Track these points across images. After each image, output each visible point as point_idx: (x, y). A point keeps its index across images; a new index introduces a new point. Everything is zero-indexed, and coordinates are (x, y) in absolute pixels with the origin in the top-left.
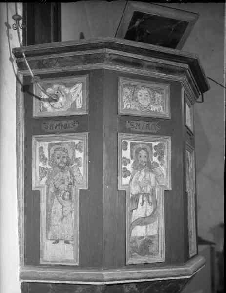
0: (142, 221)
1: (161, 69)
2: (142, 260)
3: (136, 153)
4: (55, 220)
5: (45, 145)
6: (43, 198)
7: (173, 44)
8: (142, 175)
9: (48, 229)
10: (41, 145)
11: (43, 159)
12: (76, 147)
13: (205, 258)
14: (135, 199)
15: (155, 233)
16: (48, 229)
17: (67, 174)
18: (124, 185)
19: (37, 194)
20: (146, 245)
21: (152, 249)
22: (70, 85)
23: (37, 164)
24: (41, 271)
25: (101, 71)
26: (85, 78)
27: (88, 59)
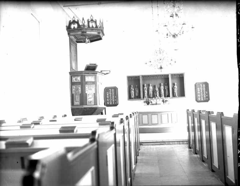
0: (90, 98)
1: (92, 73)
2: (90, 104)
3: (89, 88)
4: (76, 98)
5: (74, 86)
6: (74, 94)
7: (94, 70)
8: (144, 100)
9: (75, 100)
10: (74, 87)
11: (74, 89)
12: (79, 87)
13: (208, 164)
14: (89, 95)
15: (92, 100)
16: (75, 100)
17: (78, 91)
18: (157, 114)
19: (73, 94)
20: (91, 102)
21: (92, 103)
22: (78, 77)
23: (73, 90)
24: (75, 106)
25: (82, 75)
26: (80, 76)
27: (81, 73)
